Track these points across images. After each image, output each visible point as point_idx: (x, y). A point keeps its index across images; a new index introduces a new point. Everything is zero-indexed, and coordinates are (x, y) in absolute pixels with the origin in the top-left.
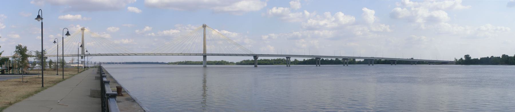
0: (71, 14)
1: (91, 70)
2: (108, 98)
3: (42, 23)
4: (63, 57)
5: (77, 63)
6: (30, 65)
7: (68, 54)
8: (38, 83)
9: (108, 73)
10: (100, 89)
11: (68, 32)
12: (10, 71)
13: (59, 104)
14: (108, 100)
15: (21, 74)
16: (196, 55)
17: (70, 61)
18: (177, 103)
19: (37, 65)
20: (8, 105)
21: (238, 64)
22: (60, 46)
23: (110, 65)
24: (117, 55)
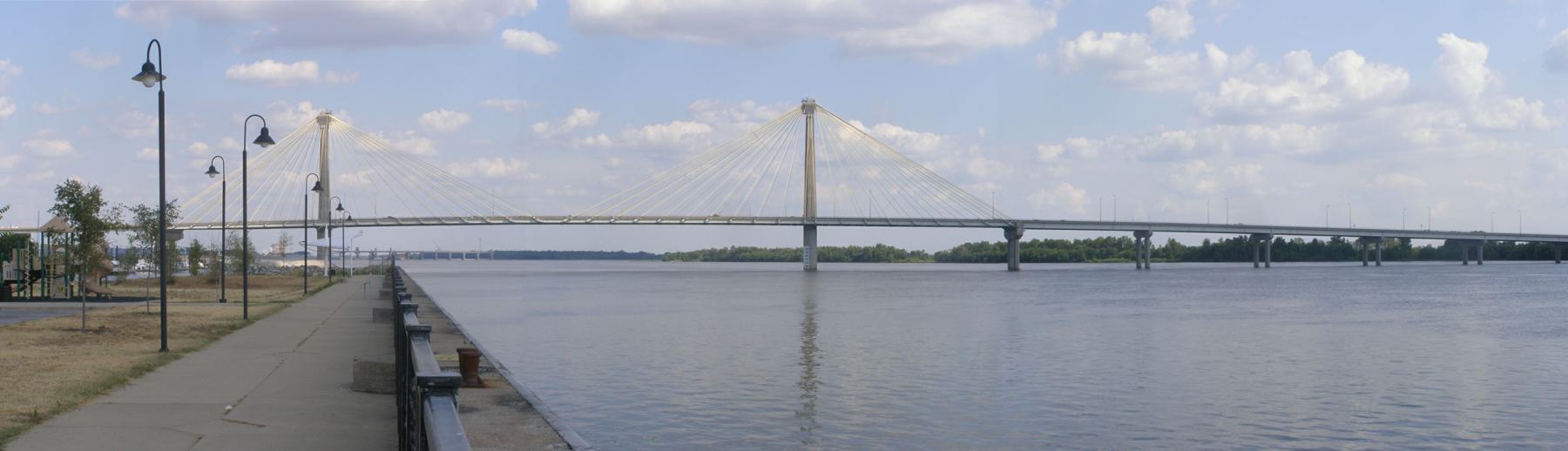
0: (277, 60)
1: (354, 283)
2: (425, 396)
3: (161, 94)
4: (245, 229)
5: (300, 253)
6: (115, 262)
7: (264, 220)
8: (148, 333)
9: (425, 296)
10: (390, 359)
11: (264, 131)
12: (34, 285)
13: (229, 421)
14: (426, 403)
15: (78, 299)
16: (776, 222)
17: (273, 246)
18: (699, 416)
19: (141, 263)
20: (24, 421)
21: (941, 258)
22: (235, 186)
23: (430, 262)
24: (462, 222)
